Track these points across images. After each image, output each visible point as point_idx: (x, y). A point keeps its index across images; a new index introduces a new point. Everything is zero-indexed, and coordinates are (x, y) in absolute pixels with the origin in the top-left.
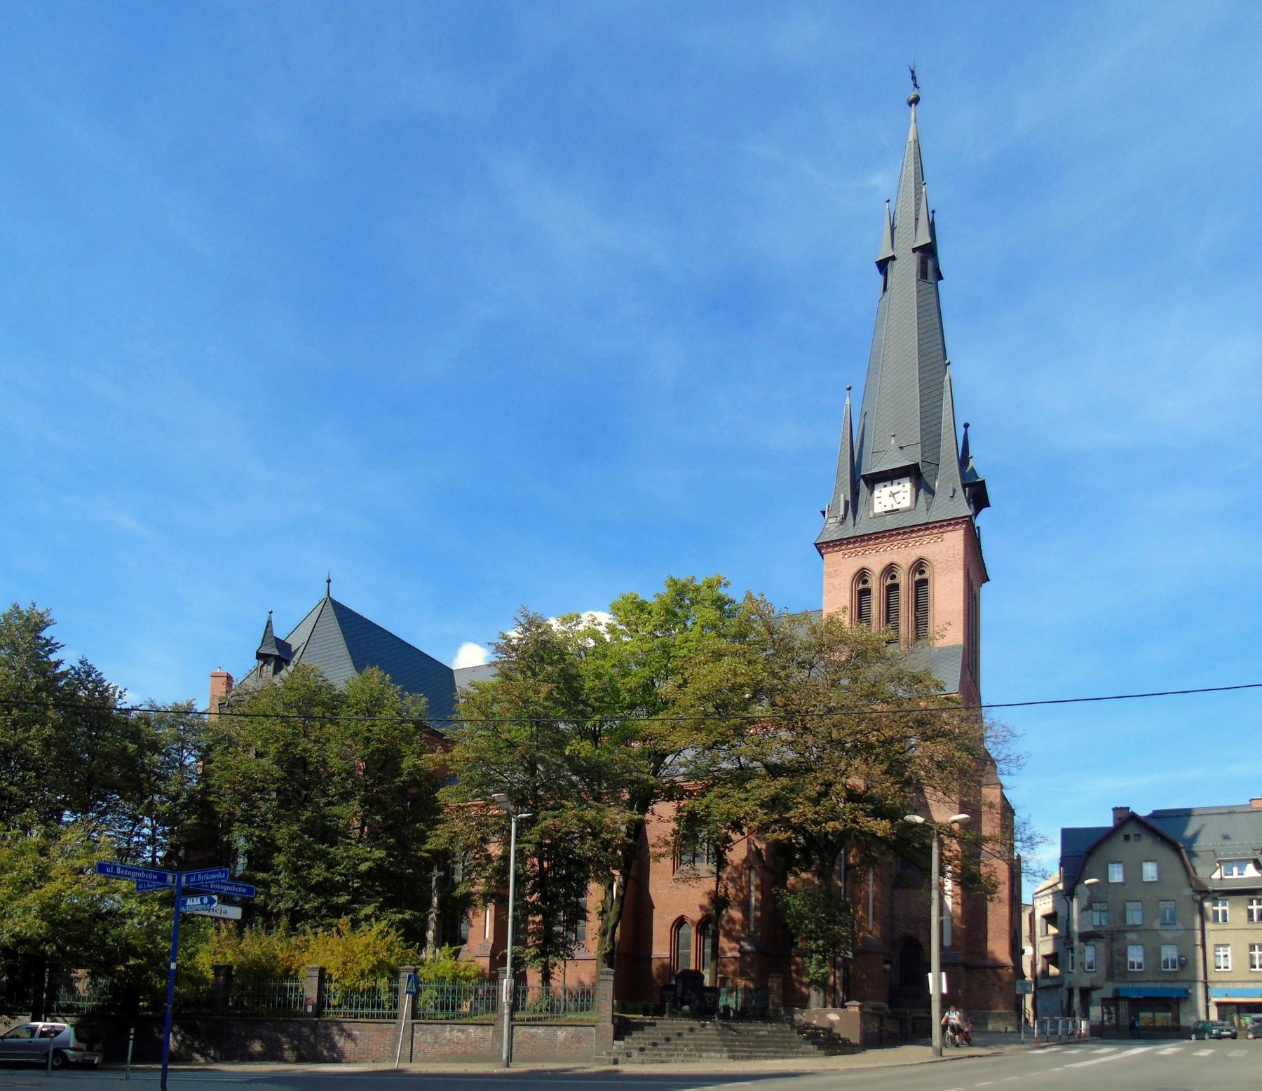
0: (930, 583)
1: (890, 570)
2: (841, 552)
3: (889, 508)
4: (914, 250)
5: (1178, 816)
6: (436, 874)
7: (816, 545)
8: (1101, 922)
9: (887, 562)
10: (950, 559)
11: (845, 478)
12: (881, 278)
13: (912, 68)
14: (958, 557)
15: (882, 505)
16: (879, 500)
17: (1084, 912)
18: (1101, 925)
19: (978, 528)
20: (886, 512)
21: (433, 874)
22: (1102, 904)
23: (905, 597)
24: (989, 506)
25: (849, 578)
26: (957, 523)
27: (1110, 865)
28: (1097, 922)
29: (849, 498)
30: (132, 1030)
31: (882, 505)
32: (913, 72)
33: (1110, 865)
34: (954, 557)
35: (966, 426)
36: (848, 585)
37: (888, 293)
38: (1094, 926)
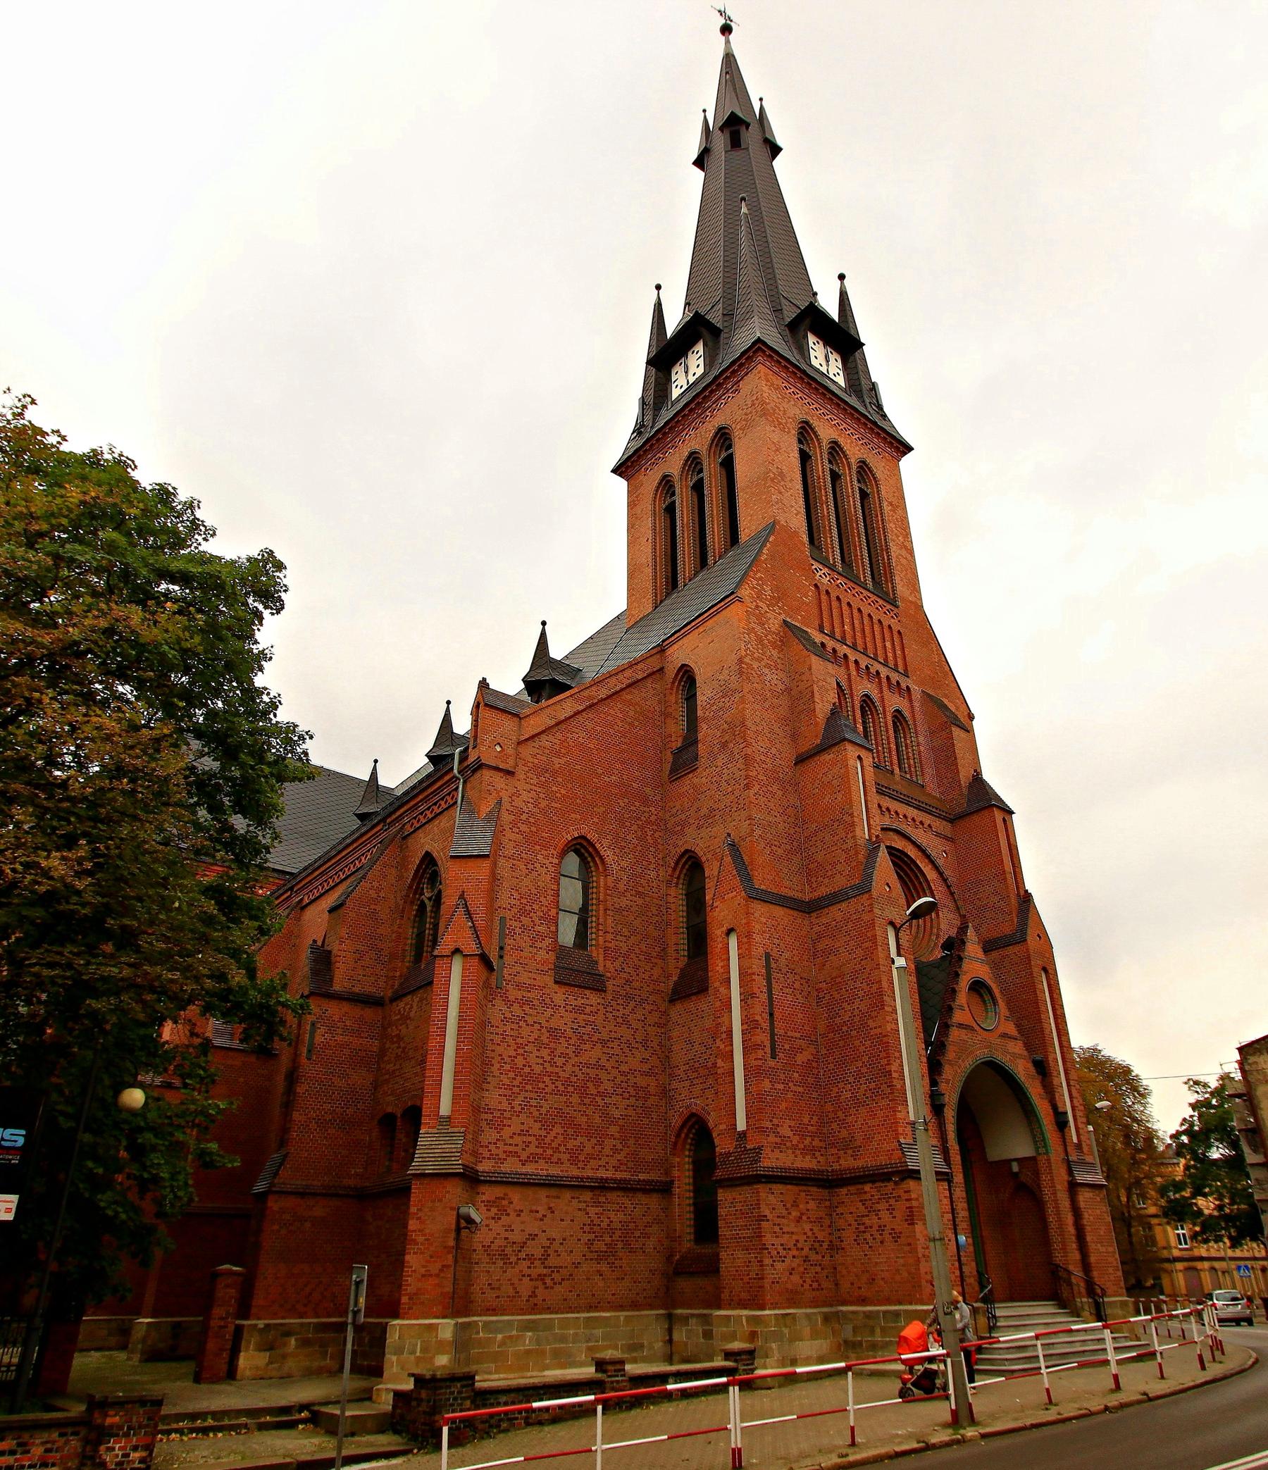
34: (753, 405)
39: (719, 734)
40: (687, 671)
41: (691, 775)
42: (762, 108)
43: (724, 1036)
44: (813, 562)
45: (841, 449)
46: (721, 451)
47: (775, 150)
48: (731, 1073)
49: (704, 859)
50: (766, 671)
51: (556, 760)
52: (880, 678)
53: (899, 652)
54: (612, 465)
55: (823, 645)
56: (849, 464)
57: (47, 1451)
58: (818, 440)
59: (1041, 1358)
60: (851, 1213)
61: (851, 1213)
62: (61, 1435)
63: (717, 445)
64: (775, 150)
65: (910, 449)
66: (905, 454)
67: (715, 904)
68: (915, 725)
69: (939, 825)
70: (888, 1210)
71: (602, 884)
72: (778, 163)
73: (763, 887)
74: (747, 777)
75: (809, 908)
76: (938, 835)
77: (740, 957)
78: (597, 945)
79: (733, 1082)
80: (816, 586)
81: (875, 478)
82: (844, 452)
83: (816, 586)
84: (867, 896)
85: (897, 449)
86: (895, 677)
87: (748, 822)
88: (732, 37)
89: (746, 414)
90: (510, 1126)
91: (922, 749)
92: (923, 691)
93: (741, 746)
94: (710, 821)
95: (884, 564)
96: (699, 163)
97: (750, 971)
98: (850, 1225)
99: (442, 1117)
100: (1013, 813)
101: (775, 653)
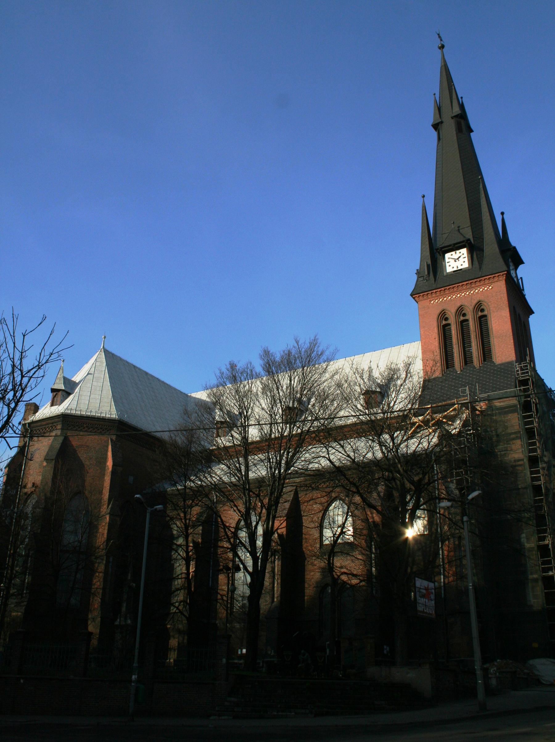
1: (460, 311)
2: (429, 300)
4: (452, 118)
6: (237, 559)
12: (435, 134)
13: (438, 33)
15: (451, 267)
16: (449, 264)
19: (521, 278)
23: (472, 326)
24: (533, 313)
25: (436, 317)
29: (430, 262)
30: (172, 658)
31: (451, 267)
32: (438, 34)
35: (502, 213)
36: (435, 324)
37: (441, 141)
64: (472, 131)
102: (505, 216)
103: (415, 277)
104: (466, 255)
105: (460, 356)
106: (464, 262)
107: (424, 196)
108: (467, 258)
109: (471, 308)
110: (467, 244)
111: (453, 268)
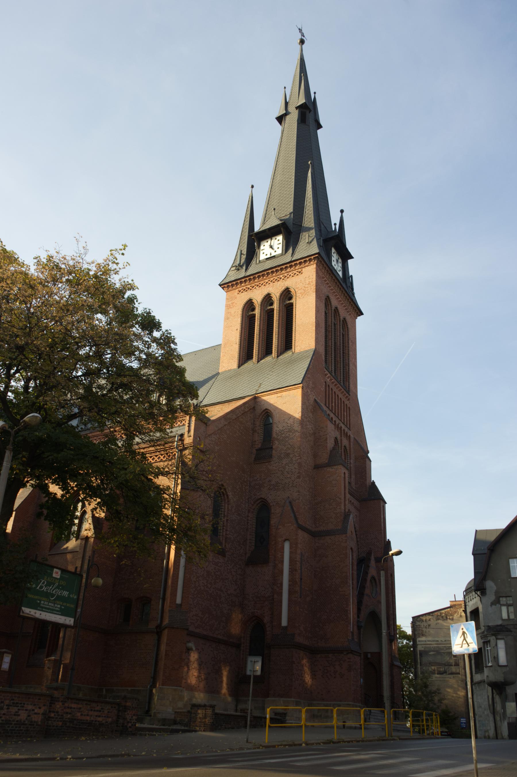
0: (294, 305)
1: (268, 299)
2: (237, 290)
3: (269, 256)
5: (320, 408)
7: (220, 285)
8: (508, 616)
9: (265, 293)
10: (307, 286)
11: (245, 241)
14: (312, 284)
15: (265, 254)
17: (494, 606)
18: (509, 619)
19: (351, 276)
20: (267, 259)
21: (309, 677)
22: (508, 598)
26: (310, 260)
27: (511, 560)
28: (505, 616)
31: (265, 254)
33: (511, 560)
34: (309, 284)
35: (315, 93)
36: (240, 312)
38: (503, 620)
39: (285, 449)
40: (267, 412)
41: (267, 464)
42: (315, 98)
43: (279, 585)
44: (325, 370)
45: (338, 311)
46: (286, 298)
47: (319, 126)
48: (281, 602)
49: (271, 504)
50: (308, 423)
51: (216, 448)
52: (341, 430)
53: (348, 418)
54: (219, 281)
55: (329, 415)
56: (340, 319)
57: (108, 712)
58: (331, 306)
59: (434, 715)
60: (321, 665)
61: (321, 665)
62: (112, 707)
63: (284, 295)
64: (319, 126)
65: (362, 314)
66: (359, 316)
67: (279, 527)
68: (350, 454)
69: (356, 503)
70: (339, 665)
71: (226, 508)
72: (319, 132)
73: (301, 523)
74: (299, 473)
75: (314, 534)
76: (355, 507)
77: (291, 553)
78: (223, 535)
79: (183, 593)
80: (325, 382)
81: (347, 327)
82: (339, 313)
83: (325, 382)
84: (344, 535)
85: (359, 313)
86: (346, 429)
87: (298, 493)
88: (303, 46)
89: (305, 287)
90: (192, 611)
91: (352, 465)
92: (354, 438)
93: (297, 458)
94: (276, 488)
95: (346, 372)
96: (280, 119)
97: (295, 560)
98: (320, 670)
99: (177, 604)
100: (386, 503)
101: (311, 415)
102: (316, 95)
103: (472, 557)
104: (281, 241)
105: (326, 395)
106: (278, 248)
107: (252, 187)
108: (281, 245)
109: (278, 295)
110: (282, 229)
111: (266, 255)
